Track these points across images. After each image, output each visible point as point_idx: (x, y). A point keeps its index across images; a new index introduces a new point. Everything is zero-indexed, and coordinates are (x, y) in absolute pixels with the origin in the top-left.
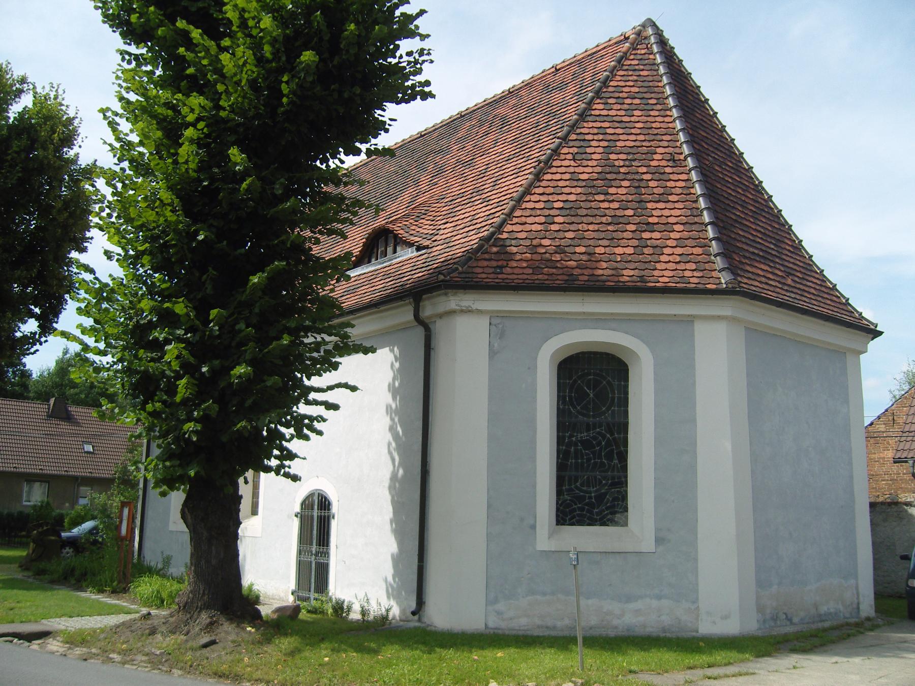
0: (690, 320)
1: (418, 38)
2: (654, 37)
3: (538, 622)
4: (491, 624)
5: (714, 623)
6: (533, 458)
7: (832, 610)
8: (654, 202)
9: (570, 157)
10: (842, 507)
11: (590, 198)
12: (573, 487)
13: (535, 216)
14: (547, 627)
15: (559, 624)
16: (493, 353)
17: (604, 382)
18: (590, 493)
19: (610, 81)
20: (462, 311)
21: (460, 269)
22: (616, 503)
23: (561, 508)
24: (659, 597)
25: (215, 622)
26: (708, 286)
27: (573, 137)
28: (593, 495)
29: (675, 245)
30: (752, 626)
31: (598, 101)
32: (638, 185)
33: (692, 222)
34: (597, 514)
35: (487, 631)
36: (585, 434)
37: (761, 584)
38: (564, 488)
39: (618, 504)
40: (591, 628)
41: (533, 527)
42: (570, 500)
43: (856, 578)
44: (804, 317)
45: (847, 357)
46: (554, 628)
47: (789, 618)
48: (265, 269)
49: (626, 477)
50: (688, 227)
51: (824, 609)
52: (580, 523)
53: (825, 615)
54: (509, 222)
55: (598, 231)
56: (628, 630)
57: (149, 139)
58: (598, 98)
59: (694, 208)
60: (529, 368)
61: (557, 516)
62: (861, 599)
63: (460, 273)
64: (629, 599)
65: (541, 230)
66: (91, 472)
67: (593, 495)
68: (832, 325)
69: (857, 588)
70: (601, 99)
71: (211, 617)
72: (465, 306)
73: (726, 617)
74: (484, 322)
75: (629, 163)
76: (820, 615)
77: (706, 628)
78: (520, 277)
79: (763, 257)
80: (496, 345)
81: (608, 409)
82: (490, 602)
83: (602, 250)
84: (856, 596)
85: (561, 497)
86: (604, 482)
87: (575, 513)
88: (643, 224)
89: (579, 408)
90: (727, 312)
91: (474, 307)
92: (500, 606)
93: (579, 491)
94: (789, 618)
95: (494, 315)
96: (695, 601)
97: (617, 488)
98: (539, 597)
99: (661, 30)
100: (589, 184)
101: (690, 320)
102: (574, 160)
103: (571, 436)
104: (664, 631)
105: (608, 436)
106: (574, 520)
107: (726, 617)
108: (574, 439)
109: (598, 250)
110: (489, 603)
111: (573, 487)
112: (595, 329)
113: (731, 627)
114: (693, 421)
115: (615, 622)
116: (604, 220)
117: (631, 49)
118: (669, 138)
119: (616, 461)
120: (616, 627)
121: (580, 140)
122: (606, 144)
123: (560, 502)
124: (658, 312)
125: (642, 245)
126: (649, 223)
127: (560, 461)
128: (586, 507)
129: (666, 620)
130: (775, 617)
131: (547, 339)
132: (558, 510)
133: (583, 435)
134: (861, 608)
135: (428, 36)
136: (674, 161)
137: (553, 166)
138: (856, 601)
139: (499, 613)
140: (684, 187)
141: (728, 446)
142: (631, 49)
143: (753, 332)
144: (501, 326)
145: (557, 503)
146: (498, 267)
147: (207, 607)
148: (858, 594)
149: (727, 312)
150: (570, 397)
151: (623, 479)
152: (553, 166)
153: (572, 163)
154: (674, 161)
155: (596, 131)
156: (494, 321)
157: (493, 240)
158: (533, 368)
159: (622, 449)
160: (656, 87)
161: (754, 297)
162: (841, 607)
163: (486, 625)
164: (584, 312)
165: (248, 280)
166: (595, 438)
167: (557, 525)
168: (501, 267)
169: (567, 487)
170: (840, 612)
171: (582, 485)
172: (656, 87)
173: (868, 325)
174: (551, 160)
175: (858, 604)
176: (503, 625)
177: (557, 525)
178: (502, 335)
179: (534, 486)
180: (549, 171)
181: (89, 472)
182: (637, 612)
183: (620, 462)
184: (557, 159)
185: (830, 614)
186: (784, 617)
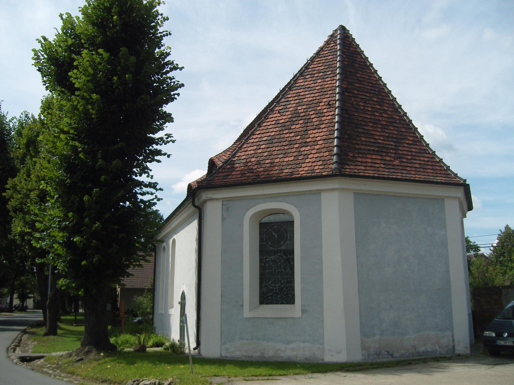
0: (319, 192)
1: (179, 69)
2: (340, 36)
3: (245, 354)
4: (223, 355)
5: (332, 355)
6: (242, 271)
7: (429, 350)
8: (312, 130)
9: (277, 112)
10: (439, 289)
11: (282, 133)
12: (267, 284)
13: (252, 146)
14: (249, 357)
15: (255, 355)
16: (223, 219)
17: (282, 229)
18: (276, 287)
19: (311, 65)
20: (209, 200)
21: (208, 178)
22: (289, 292)
23: (262, 295)
24: (304, 342)
25: (90, 351)
26: (323, 174)
27: (283, 100)
28: (277, 288)
29: (315, 152)
30: (358, 357)
31: (302, 78)
32: (308, 121)
33: (328, 139)
34: (280, 298)
35: (222, 358)
36: (273, 257)
37: (364, 334)
38: (263, 285)
39: (290, 293)
40: (270, 357)
41: (242, 306)
42: (266, 291)
43: (452, 331)
44: (396, 182)
45: (445, 201)
46: (252, 357)
47: (390, 353)
48: (92, 192)
49: (294, 278)
50: (326, 141)
51: (422, 349)
52: (271, 303)
53: (423, 352)
54: (240, 151)
55: (280, 150)
56: (289, 359)
57: (49, 141)
58: (301, 76)
59: (332, 130)
60: (240, 225)
61: (260, 300)
62: (456, 343)
63: (208, 181)
64: (289, 342)
65: (253, 153)
66: (133, 286)
67: (277, 288)
68: (419, 184)
69: (453, 336)
70: (303, 76)
71: (89, 349)
72: (209, 197)
73: (338, 353)
74: (219, 204)
75: (306, 110)
76: (419, 353)
77: (328, 358)
78: (231, 180)
79: (377, 151)
80: (225, 215)
81: (285, 243)
82: (222, 344)
83: (278, 160)
84: (452, 341)
85: (262, 290)
86: (283, 281)
87: (269, 298)
88: (303, 143)
89: (270, 243)
90: (336, 186)
91: (213, 197)
92: (227, 346)
93: (271, 286)
94: (390, 353)
95: (224, 200)
96: (322, 344)
97: (289, 284)
98: (245, 341)
99: (347, 30)
100: (284, 125)
101: (319, 192)
102: (279, 113)
103: (267, 258)
104: (306, 359)
105: (285, 257)
106: (268, 302)
107: (338, 353)
108: (267, 259)
109: (276, 161)
110: (222, 344)
111: (267, 284)
112: (271, 202)
113: (342, 358)
114: (321, 247)
115: (282, 354)
116: (284, 144)
117: (327, 45)
118: (331, 92)
119: (289, 270)
120: (282, 357)
121: (286, 101)
122: (298, 101)
123: (261, 292)
124: (304, 190)
125: (300, 153)
126: (306, 142)
127: (261, 271)
128: (274, 295)
129: (308, 354)
130: (378, 353)
131: (248, 209)
132: (260, 297)
133: (272, 257)
134: (456, 348)
135: (183, 68)
136: (330, 105)
137: (269, 118)
138: (452, 345)
139: (227, 349)
140: (331, 119)
141: (339, 259)
142: (327, 45)
143: (358, 194)
144: (227, 205)
145: (260, 293)
146: (225, 176)
147: (89, 344)
148: (453, 341)
149: (336, 186)
150: (266, 238)
151: (292, 279)
152: (269, 118)
153: (279, 115)
154: (330, 105)
155: (295, 95)
156: (225, 203)
157: (229, 162)
158: (241, 225)
159: (292, 263)
160: (333, 64)
161: (350, 176)
162: (437, 348)
163: (221, 355)
164: (265, 194)
165: (84, 200)
166: (278, 258)
167: (260, 304)
168: (227, 176)
169: (265, 284)
170: (437, 351)
171: (272, 283)
172: (333, 64)
173: (459, 181)
174: (269, 115)
175: (454, 346)
176: (228, 355)
177: (260, 304)
178: (228, 210)
179: (242, 285)
180: (266, 121)
181: (132, 286)
182: (293, 349)
183: (290, 271)
184: (271, 114)
185: (428, 352)
186: (386, 353)
